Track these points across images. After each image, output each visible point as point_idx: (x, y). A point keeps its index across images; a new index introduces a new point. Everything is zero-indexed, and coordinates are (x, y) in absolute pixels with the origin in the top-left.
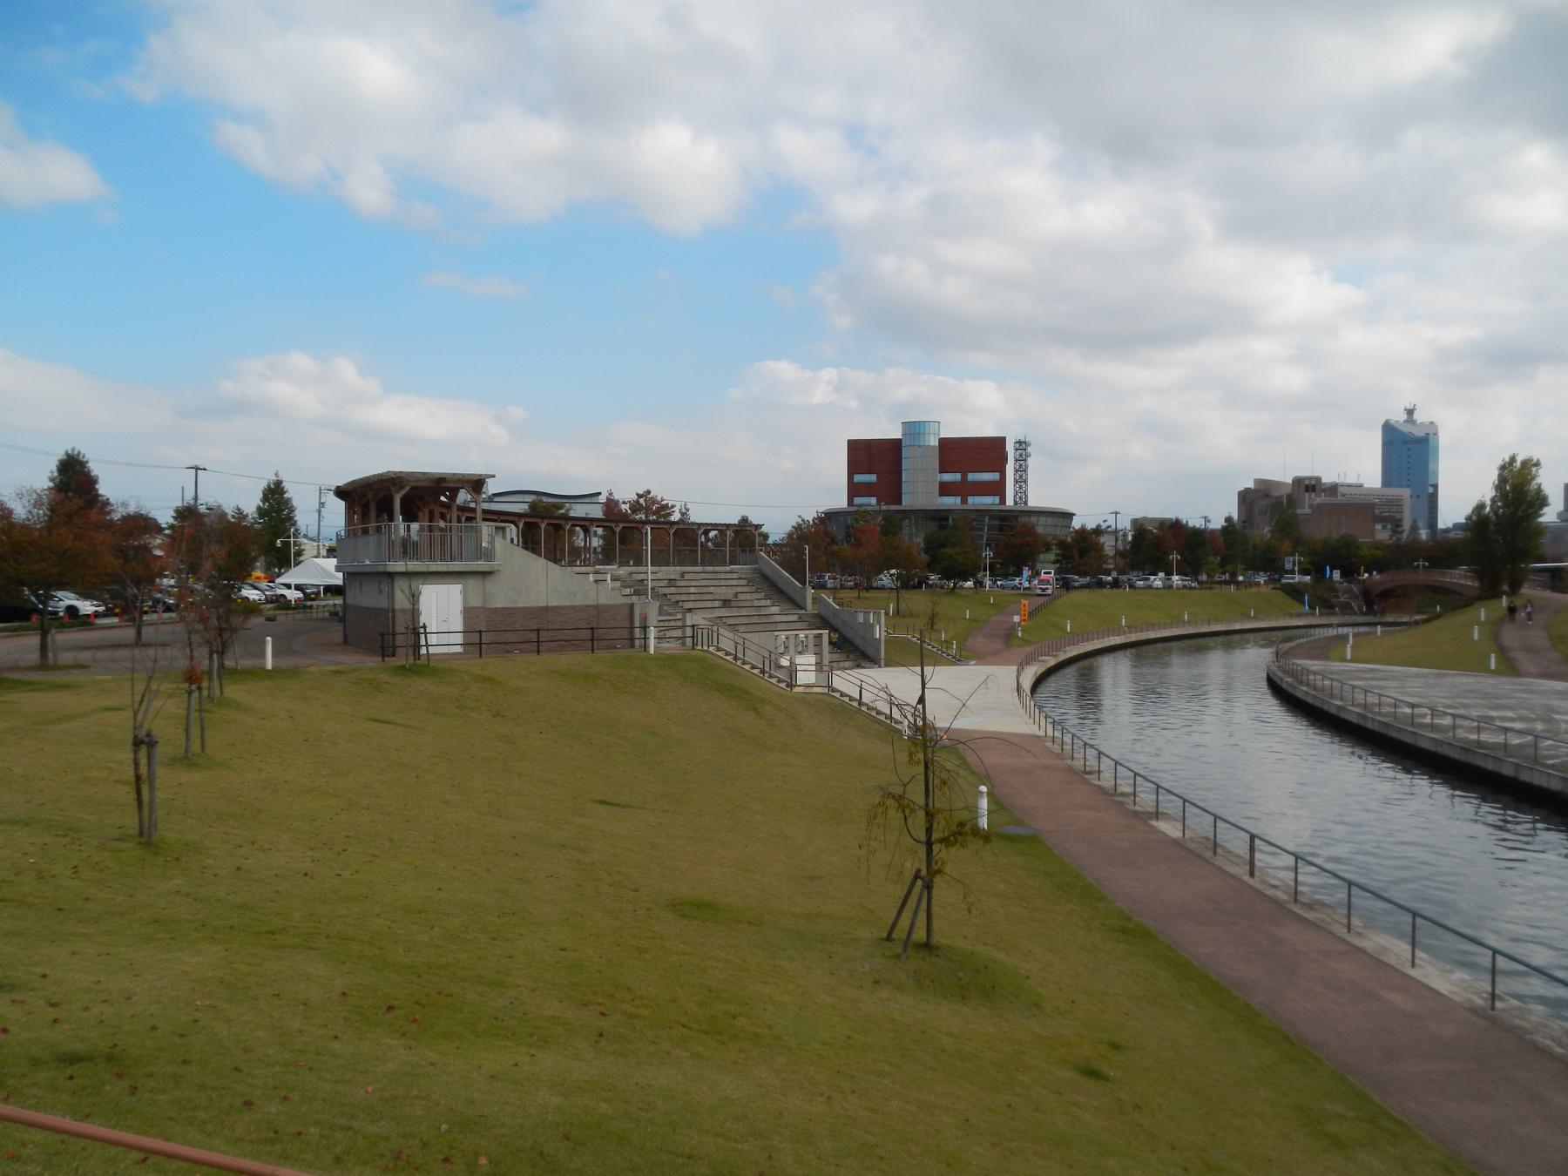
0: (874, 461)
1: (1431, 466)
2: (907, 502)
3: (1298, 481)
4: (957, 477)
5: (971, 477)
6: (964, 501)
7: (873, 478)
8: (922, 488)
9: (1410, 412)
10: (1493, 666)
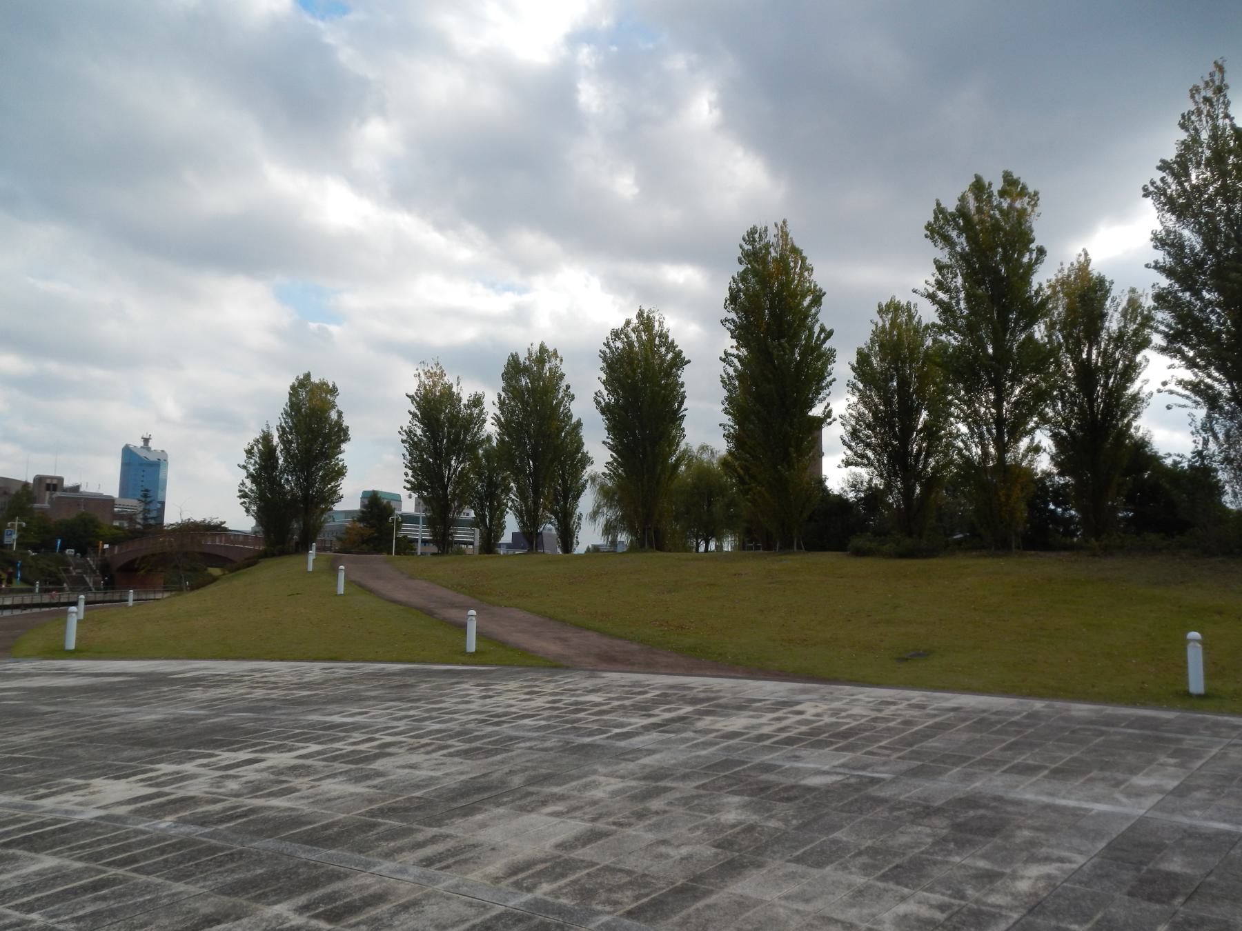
1: (161, 475)
3: (39, 480)
9: (146, 440)
10: (1196, 682)
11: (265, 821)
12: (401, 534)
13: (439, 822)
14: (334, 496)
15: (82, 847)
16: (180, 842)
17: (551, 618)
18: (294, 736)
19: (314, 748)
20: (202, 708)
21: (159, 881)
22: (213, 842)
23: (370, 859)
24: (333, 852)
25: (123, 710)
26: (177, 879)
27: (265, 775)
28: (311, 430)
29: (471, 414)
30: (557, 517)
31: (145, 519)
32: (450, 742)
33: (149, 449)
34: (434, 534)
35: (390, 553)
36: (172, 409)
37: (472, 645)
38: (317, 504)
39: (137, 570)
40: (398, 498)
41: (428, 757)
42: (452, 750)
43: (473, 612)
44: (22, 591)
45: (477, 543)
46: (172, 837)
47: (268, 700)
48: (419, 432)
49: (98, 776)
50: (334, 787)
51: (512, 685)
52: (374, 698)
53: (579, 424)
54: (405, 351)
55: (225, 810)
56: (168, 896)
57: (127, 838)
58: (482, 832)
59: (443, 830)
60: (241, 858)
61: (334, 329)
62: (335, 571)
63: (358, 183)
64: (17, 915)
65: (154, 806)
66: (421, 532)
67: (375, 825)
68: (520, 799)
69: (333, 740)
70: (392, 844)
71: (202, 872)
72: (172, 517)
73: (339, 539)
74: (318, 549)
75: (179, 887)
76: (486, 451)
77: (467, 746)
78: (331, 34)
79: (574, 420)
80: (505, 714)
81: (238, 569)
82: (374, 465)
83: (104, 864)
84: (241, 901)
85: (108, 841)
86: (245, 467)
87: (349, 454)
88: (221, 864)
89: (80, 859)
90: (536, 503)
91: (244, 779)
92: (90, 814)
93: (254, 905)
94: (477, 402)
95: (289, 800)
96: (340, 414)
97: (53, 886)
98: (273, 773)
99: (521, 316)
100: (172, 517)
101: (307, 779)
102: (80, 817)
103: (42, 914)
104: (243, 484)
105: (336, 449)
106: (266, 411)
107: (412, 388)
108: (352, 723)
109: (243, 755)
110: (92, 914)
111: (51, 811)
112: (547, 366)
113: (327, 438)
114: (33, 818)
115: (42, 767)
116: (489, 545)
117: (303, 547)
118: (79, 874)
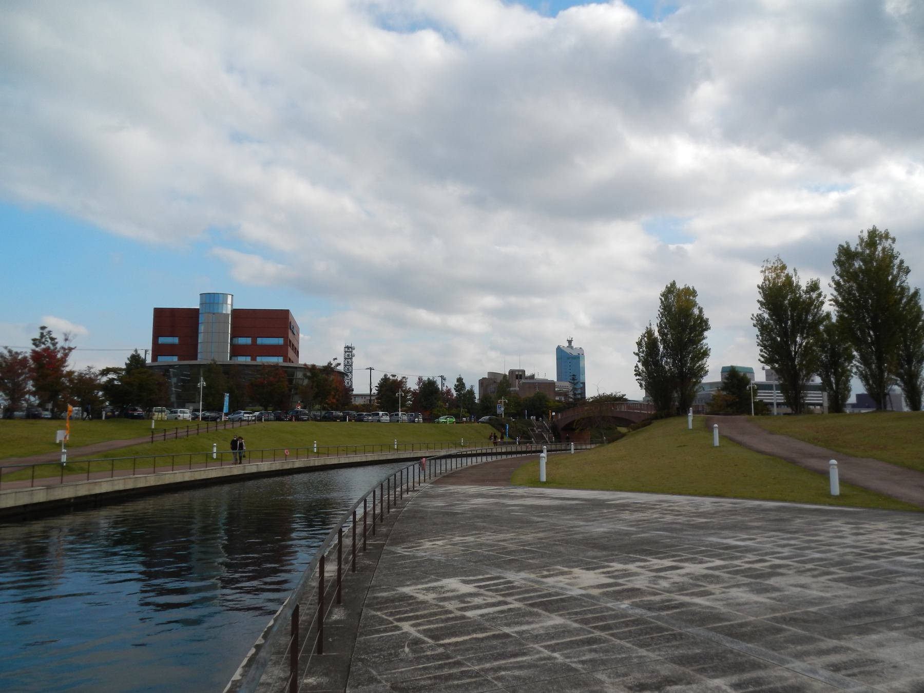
0: (174, 325)
2: (203, 357)
3: (512, 372)
4: (247, 341)
5: (260, 341)
6: (254, 359)
7: (175, 340)
8: (215, 347)
9: (570, 342)
11: (693, 613)
12: (758, 398)
13: (837, 636)
14: (702, 371)
15: (576, 613)
16: (637, 620)
17: (910, 468)
18: (701, 552)
19: (718, 563)
20: (631, 526)
21: (629, 645)
22: (659, 623)
23: (783, 657)
24: (750, 645)
25: (582, 523)
26: (641, 646)
27: (685, 579)
28: (681, 323)
29: (810, 298)
30: (902, 380)
31: (575, 394)
32: (832, 569)
33: (572, 348)
34: (787, 398)
35: (750, 413)
36: (584, 319)
37: (836, 489)
38: (690, 378)
39: (574, 430)
40: (750, 371)
41: (815, 580)
42: (836, 576)
43: (833, 462)
44: (509, 443)
45: (826, 404)
46: (631, 615)
47: (677, 523)
48: (766, 316)
49: (577, 567)
50: (740, 594)
51: (881, 525)
52: (758, 528)
53: (916, 293)
54: (747, 255)
55: (663, 601)
56: (636, 657)
57: (602, 612)
58: (881, 650)
59: (843, 643)
60: (682, 638)
61: (688, 247)
62: (710, 430)
63: (695, 134)
64: (547, 653)
65: (615, 592)
66: (776, 397)
67: (779, 630)
68: (913, 626)
69: (732, 558)
70: (799, 648)
71: (656, 644)
72: (591, 392)
73: (708, 404)
74: (694, 412)
75: (643, 652)
76: (826, 326)
77: (849, 574)
78: (665, 30)
79: (912, 291)
80: (880, 550)
81: (638, 428)
82: (733, 345)
83: (592, 627)
84: (688, 670)
85: (590, 611)
86: (637, 354)
87: (710, 339)
88: (668, 640)
89: (576, 621)
90: (879, 367)
91: (672, 580)
92: (576, 592)
93: (698, 676)
94: (814, 287)
95: (708, 600)
96: (701, 310)
97: (564, 637)
98: (691, 578)
99: (846, 210)
100: (591, 392)
101: (718, 586)
102: (570, 593)
103: (561, 655)
104: (637, 366)
105: (700, 336)
106: (648, 316)
107: (760, 280)
108: (744, 546)
109: (667, 563)
110: (591, 660)
111: (553, 587)
112: (880, 248)
113: (693, 329)
114: (543, 590)
115: (542, 557)
116: (837, 403)
117: (682, 411)
118: (578, 632)
